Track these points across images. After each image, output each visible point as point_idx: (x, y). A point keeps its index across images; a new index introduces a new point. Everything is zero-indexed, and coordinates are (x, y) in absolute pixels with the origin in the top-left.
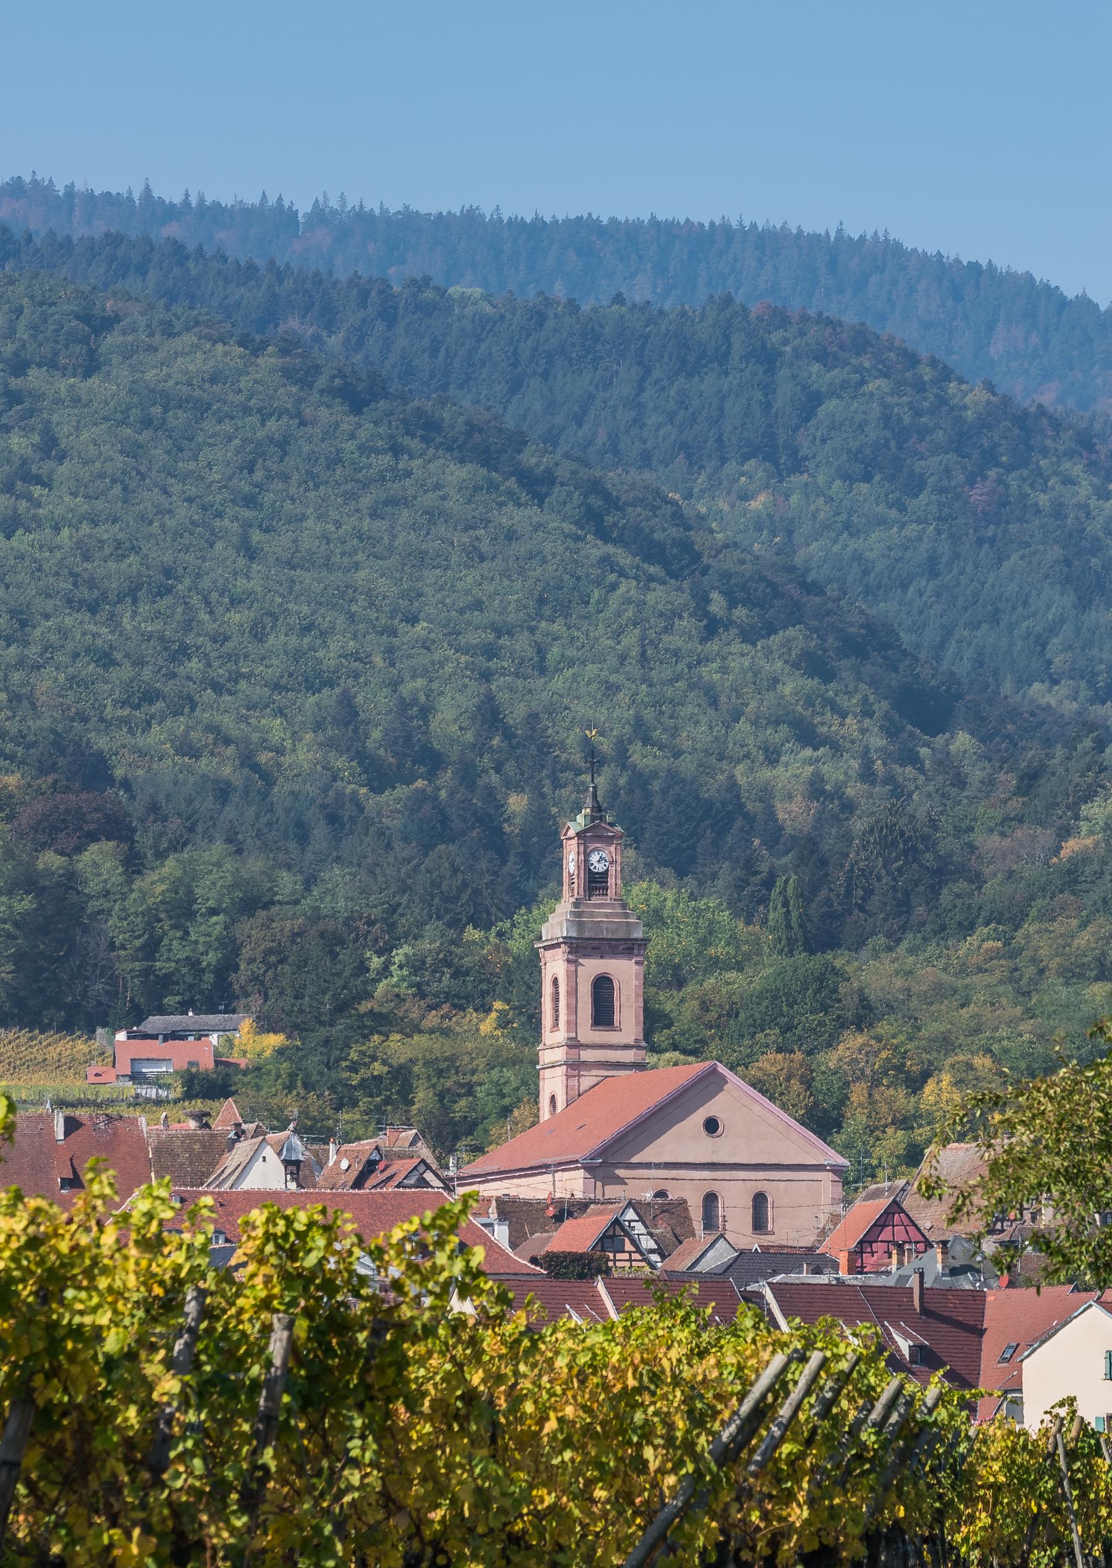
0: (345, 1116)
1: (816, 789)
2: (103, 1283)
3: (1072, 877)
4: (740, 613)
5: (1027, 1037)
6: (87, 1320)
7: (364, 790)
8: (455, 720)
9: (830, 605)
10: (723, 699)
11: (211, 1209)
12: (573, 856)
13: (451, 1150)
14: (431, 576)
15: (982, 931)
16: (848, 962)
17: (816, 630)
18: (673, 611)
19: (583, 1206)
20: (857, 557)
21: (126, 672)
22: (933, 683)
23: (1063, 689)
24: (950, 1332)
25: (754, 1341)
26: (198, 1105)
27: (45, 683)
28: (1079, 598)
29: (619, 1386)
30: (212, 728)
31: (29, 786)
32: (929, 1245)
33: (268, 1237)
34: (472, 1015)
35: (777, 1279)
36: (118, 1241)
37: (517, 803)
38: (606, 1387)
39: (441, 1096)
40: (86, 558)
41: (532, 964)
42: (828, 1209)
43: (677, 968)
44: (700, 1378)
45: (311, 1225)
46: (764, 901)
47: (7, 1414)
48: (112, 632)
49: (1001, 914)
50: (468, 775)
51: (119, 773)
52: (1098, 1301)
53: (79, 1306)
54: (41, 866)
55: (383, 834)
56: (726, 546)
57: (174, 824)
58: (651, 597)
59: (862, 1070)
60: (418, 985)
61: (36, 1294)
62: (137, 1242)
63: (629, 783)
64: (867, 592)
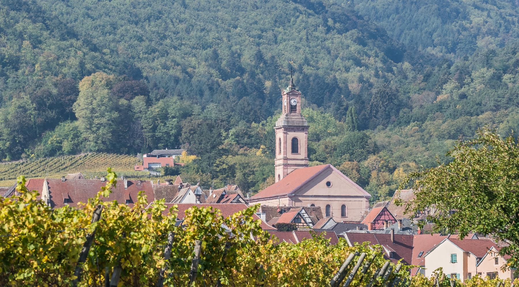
0: (214, 181)
1: (361, 80)
2: (143, 230)
3: (440, 108)
4: (338, 25)
5: (426, 157)
6: (137, 242)
7: (221, 80)
8: (249, 58)
9: (366, 23)
10: (332, 52)
11: (177, 208)
12: (285, 100)
13: (247, 191)
14: (241, 13)
15: (412, 124)
16: (371, 134)
17: (361, 31)
18: (316, 25)
19: (289, 209)
20: (374, 7)
21: (147, 43)
22: (397, 47)
23: (437, 49)
24: (402, 247)
25: (344, 249)
26: (169, 177)
27: (121, 47)
28: (443, 21)
29: (302, 263)
30: (174, 61)
31: (116, 78)
32: (396, 221)
33: (194, 217)
34: (254, 150)
35: (348, 232)
36: (147, 218)
37: (268, 84)
38: (298, 263)
39: (244, 174)
40: (134, 8)
41: (273, 134)
42: (365, 210)
43: (318, 135)
44: (327, 261)
45: (207, 213)
46: (345, 114)
47: (113, 271)
48: (142, 31)
49: (418, 118)
50: (253, 75)
51: (145, 74)
52: (448, 238)
53: (135, 238)
54: (120, 103)
55: (226, 93)
56: (333, 4)
57: (162, 90)
58: (310, 20)
59: (375, 167)
60: (237, 141)
61: (122, 234)
62: (153, 217)
63: (303, 78)
64: (377, 18)
